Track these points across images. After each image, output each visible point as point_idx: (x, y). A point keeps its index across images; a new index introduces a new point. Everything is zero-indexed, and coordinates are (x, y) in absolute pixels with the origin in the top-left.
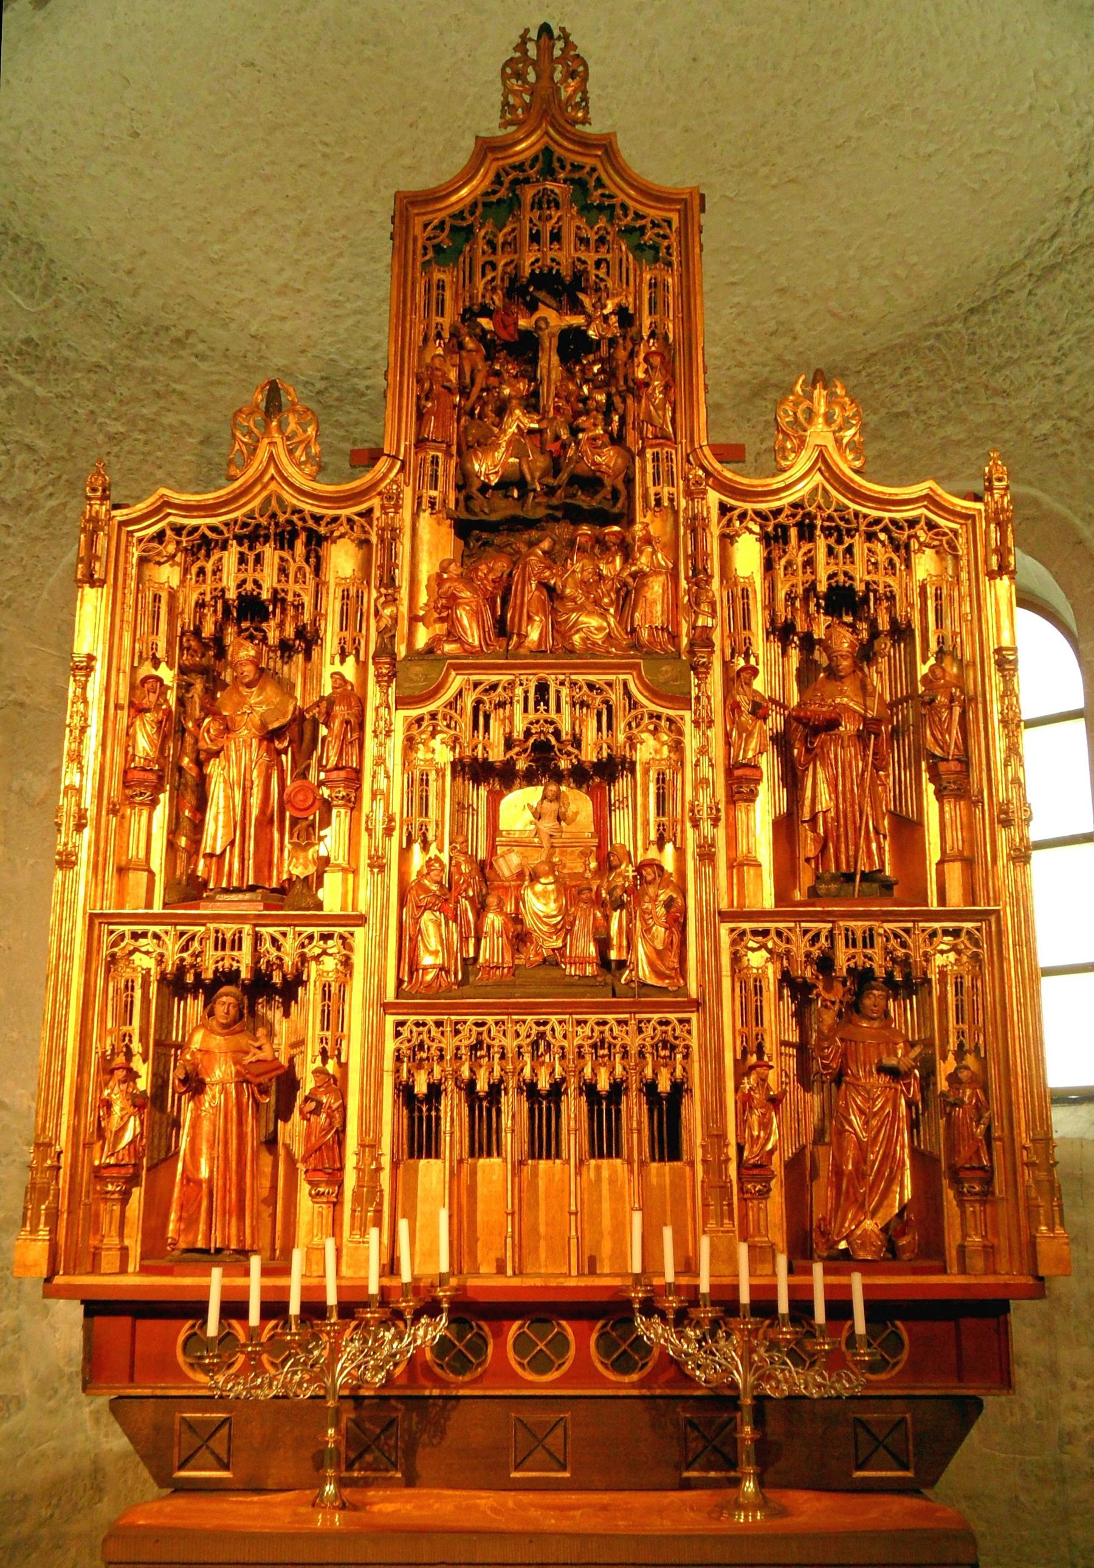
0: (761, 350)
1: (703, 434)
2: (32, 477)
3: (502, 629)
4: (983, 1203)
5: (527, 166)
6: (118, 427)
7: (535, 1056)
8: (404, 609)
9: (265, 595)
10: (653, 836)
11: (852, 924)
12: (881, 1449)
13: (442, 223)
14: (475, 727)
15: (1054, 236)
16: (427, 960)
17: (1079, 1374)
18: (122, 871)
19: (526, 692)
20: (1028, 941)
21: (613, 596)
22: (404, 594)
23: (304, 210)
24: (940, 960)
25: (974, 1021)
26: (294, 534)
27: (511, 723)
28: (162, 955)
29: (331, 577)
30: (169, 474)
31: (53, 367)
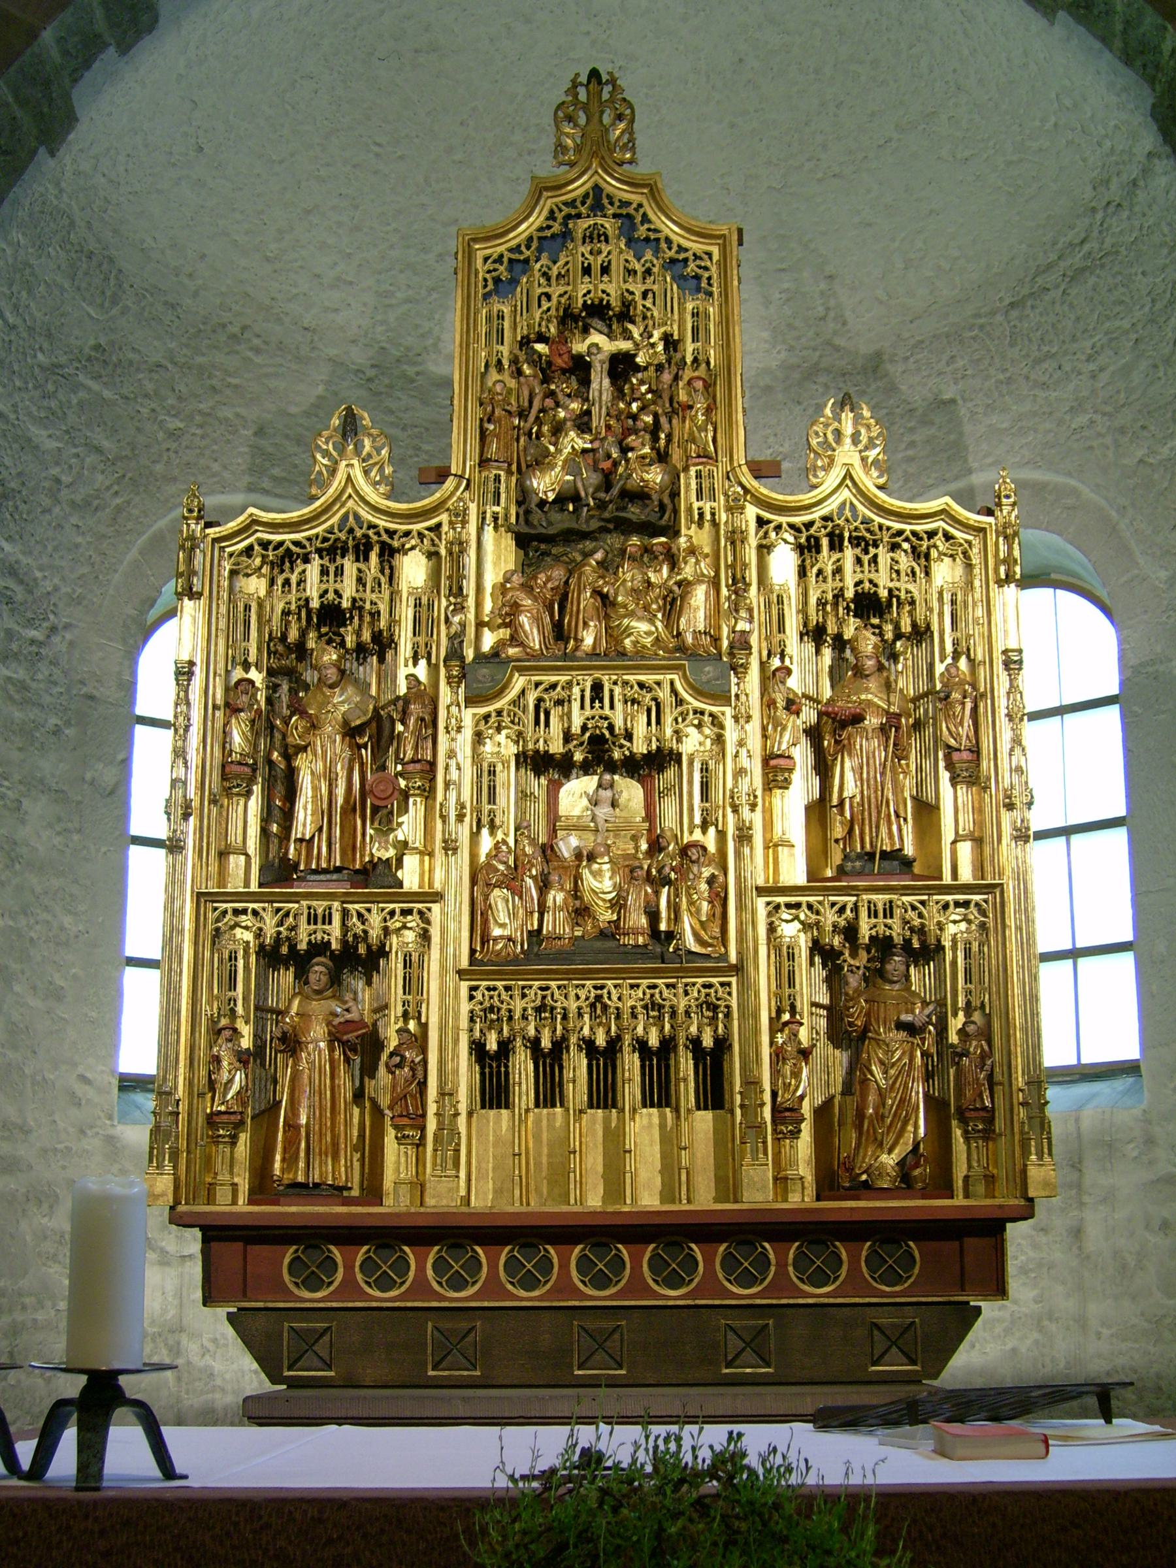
0: (811, 334)
2: (100, 477)
3: (560, 633)
5: (578, 203)
7: (594, 1016)
8: (471, 616)
9: (345, 604)
10: (698, 820)
11: (874, 897)
12: (894, 1349)
13: (501, 256)
14: (537, 723)
15: (1082, 242)
16: (496, 932)
17: (1103, 1324)
18: (223, 855)
19: (583, 691)
20: (1026, 910)
21: (661, 602)
22: (471, 602)
23: (356, 207)
26: (368, 547)
27: (570, 719)
28: (260, 929)
29: (404, 588)
30: (225, 467)
31: (119, 371)
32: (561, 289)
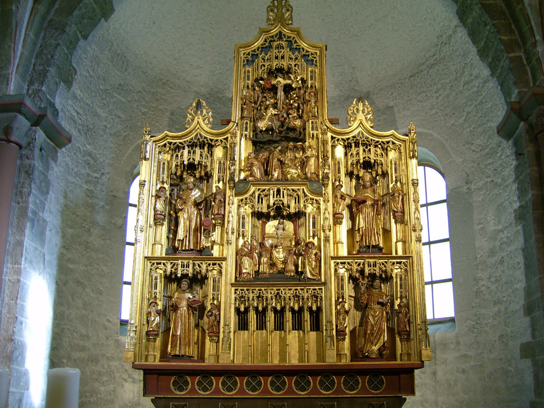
1: (326, 116)
2: (120, 126)
3: (267, 173)
4: (408, 341)
6: (144, 110)
7: (276, 299)
8: (237, 167)
9: (196, 163)
10: (311, 235)
11: (370, 260)
13: (249, 53)
14: (259, 202)
15: (434, 56)
17: (443, 404)
22: (237, 163)
23: (204, 43)
24: (395, 271)
25: (405, 288)
27: (269, 201)
29: (215, 158)
32: (268, 63)
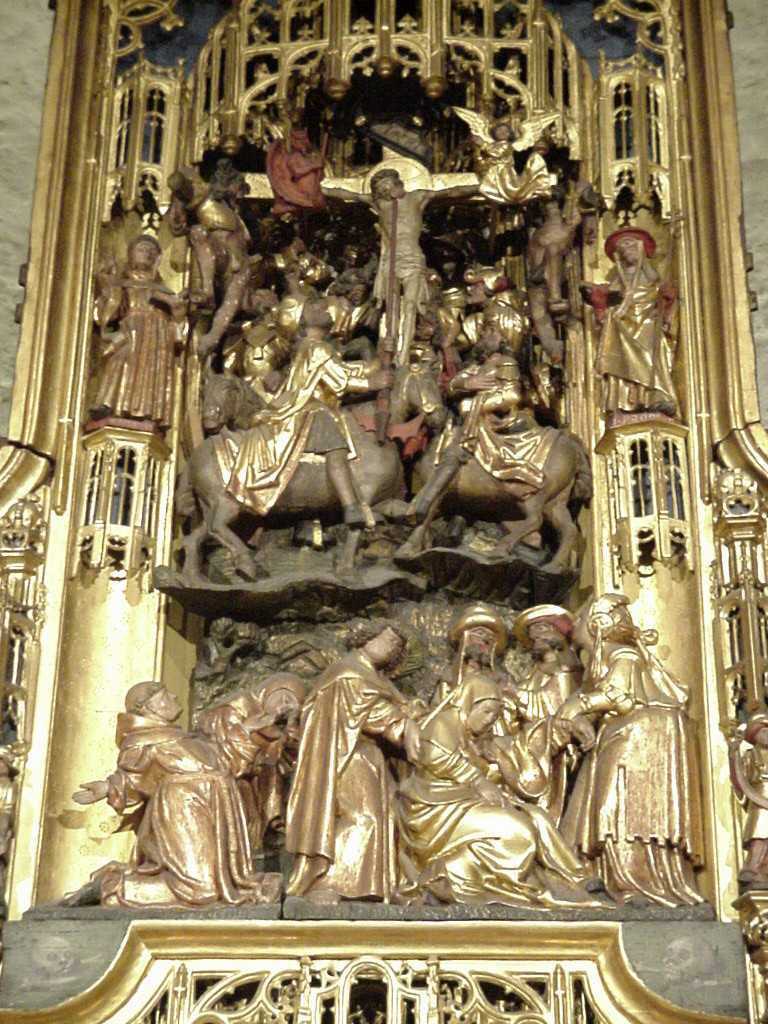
1: (750, 398)
3: (273, 850)
19: (329, 1003)
32: (301, 48)
